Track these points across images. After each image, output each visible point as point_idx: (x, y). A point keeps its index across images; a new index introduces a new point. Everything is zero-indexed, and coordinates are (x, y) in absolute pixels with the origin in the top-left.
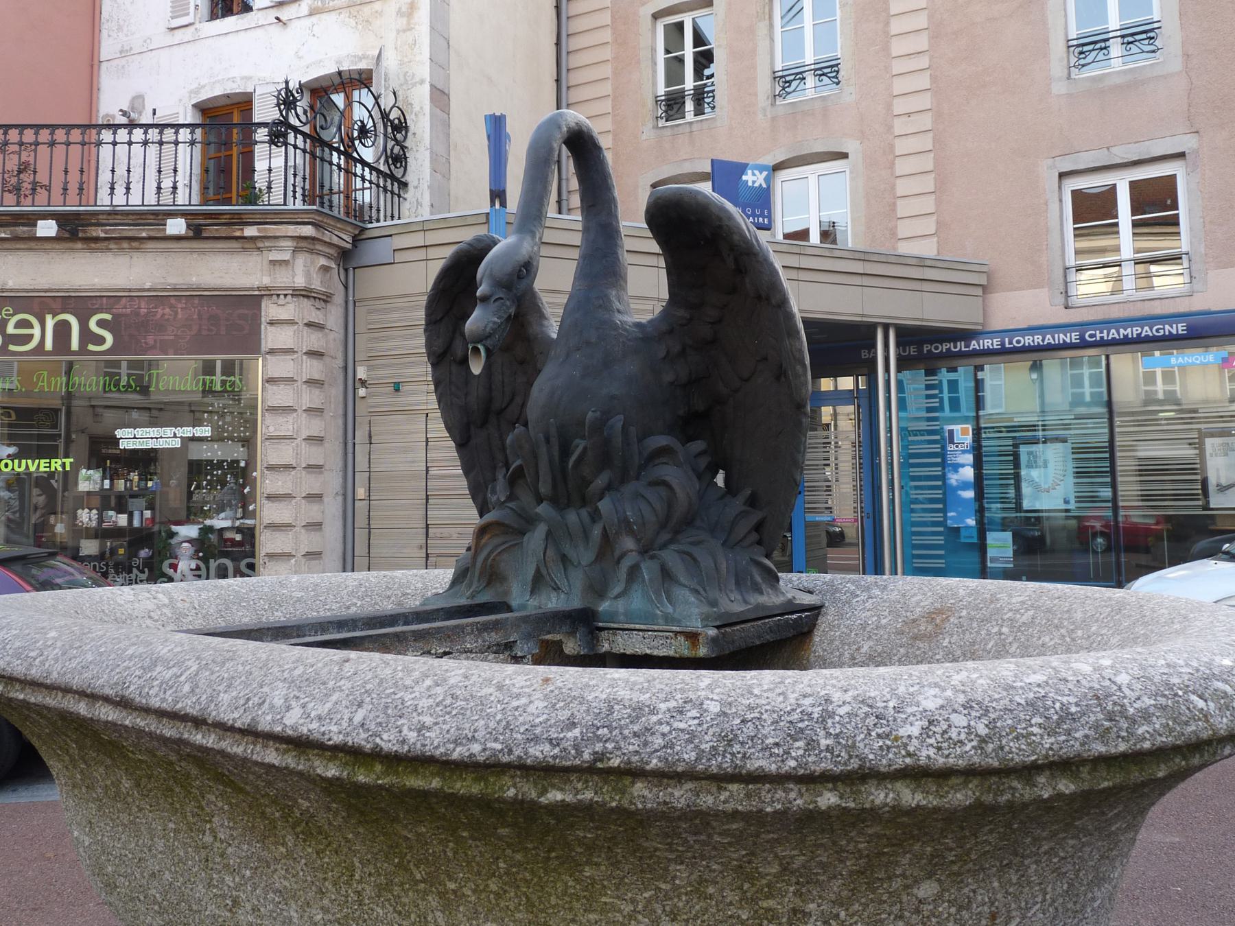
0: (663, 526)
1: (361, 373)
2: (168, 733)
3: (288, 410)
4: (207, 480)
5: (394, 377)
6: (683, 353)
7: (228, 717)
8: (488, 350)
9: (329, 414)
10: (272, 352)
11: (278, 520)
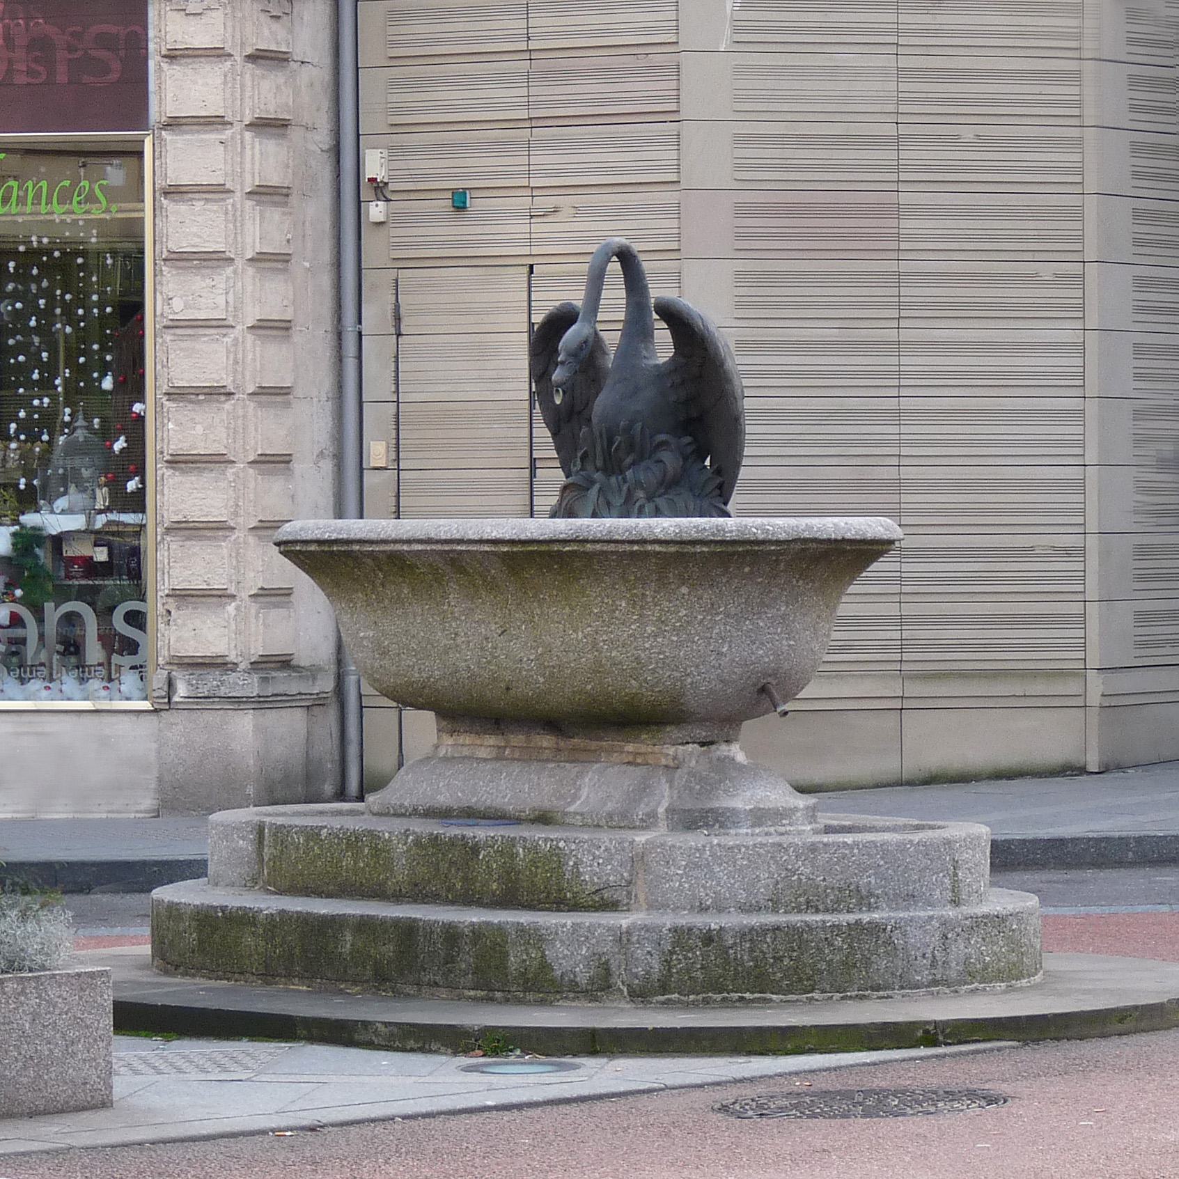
0: (661, 484)
1: (375, 166)
2: (447, 548)
3: (212, 260)
4: (17, 420)
5: (453, 176)
6: (683, 383)
7: (472, 537)
8: (564, 391)
9: (300, 265)
10: (174, 124)
11: (196, 516)
